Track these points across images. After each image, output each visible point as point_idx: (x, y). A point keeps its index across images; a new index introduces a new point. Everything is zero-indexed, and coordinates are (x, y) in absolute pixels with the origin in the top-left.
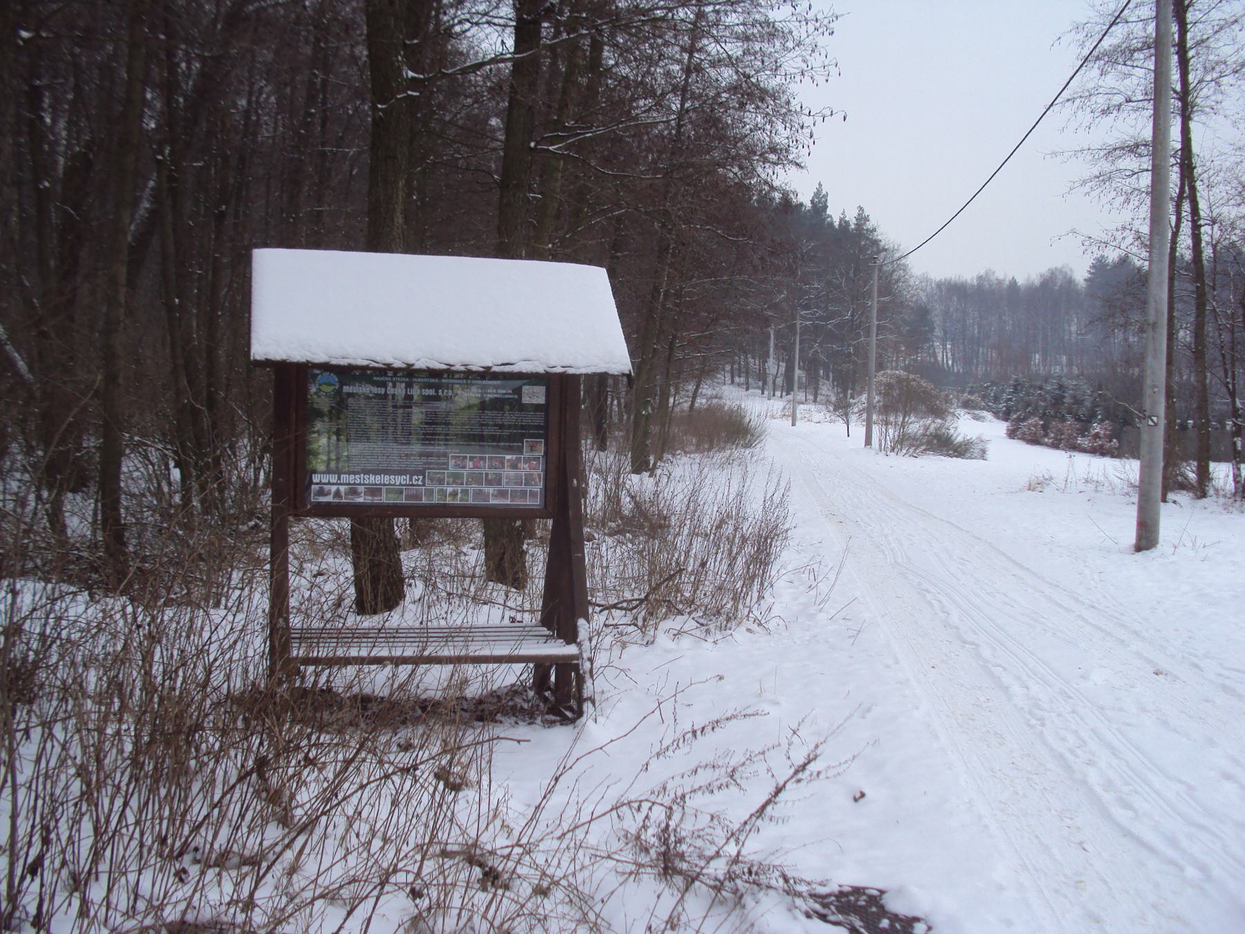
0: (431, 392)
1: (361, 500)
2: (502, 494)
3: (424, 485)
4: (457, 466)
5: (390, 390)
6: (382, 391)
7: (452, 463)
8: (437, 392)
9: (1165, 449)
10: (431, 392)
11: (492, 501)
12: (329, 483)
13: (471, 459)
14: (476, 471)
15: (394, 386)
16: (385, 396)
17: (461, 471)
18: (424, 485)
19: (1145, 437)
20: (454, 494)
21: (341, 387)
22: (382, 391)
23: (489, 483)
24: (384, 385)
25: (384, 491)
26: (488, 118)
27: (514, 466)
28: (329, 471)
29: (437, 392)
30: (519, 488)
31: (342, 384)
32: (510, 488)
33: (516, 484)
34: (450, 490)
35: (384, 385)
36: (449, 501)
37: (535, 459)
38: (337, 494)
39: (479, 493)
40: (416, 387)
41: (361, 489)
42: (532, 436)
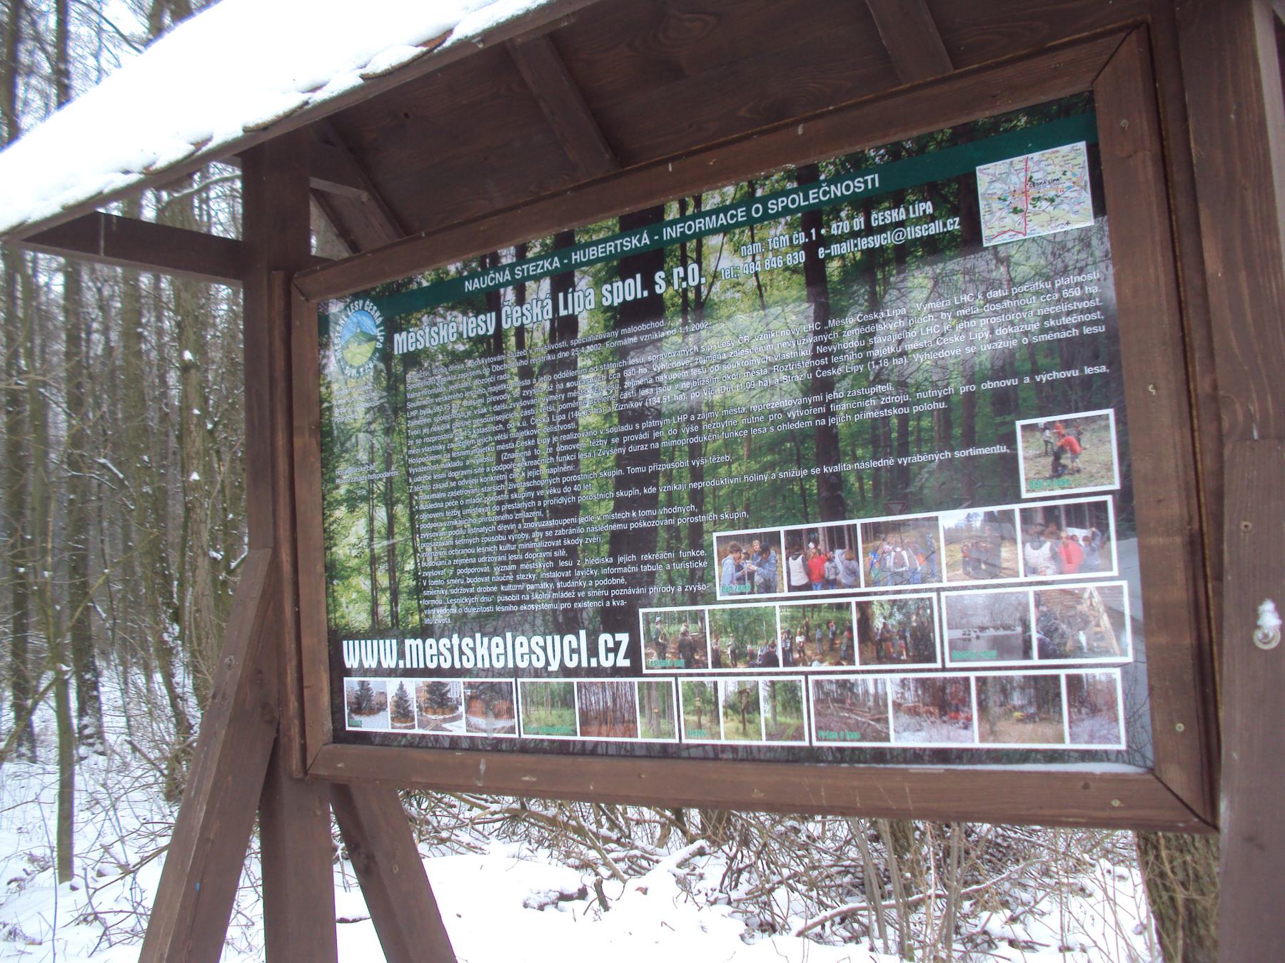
0: (630, 289)
1: (458, 729)
2: (943, 700)
3: (635, 670)
4: (744, 578)
5: (512, 316)
6: (483, 324)
7: (724, 569)
8: (649, 284)
9: (951, 750)
10: (630, 289)
11: (902, 738)
12: (379, 672)
13: (796, 543)
14: (822, 597)
15: (521, 300)
16: (493, 345)
17: (759, 602)
18: (635, 670)
19: (1145, 737)
20: (746, 705)
21: (389, 340)
22: (483, 324)
23: (879, 649)
24: (490, 301)
25: (517, 696)
26: (1183, 733)
27: (981, 561)
28: (377, 631)
29: (649, 284)
30: (1015, 669)
31: (392, 327)
32: (980, 665)
33: (1002, 647)
34: (727, 686)
35: (490, 301)
36: (727, 733)
37: (1076, 515)
38: (402, 712)
39: (841, 698)
40: (583, 282)
41: (457, 688)
42: (1054, 399)
